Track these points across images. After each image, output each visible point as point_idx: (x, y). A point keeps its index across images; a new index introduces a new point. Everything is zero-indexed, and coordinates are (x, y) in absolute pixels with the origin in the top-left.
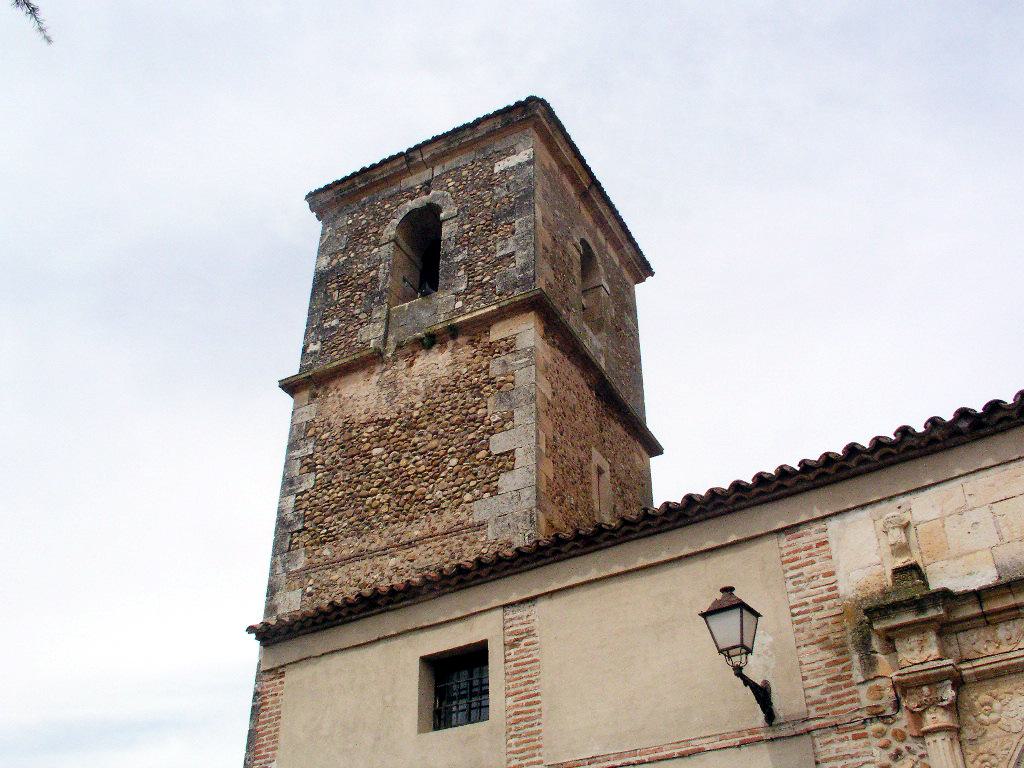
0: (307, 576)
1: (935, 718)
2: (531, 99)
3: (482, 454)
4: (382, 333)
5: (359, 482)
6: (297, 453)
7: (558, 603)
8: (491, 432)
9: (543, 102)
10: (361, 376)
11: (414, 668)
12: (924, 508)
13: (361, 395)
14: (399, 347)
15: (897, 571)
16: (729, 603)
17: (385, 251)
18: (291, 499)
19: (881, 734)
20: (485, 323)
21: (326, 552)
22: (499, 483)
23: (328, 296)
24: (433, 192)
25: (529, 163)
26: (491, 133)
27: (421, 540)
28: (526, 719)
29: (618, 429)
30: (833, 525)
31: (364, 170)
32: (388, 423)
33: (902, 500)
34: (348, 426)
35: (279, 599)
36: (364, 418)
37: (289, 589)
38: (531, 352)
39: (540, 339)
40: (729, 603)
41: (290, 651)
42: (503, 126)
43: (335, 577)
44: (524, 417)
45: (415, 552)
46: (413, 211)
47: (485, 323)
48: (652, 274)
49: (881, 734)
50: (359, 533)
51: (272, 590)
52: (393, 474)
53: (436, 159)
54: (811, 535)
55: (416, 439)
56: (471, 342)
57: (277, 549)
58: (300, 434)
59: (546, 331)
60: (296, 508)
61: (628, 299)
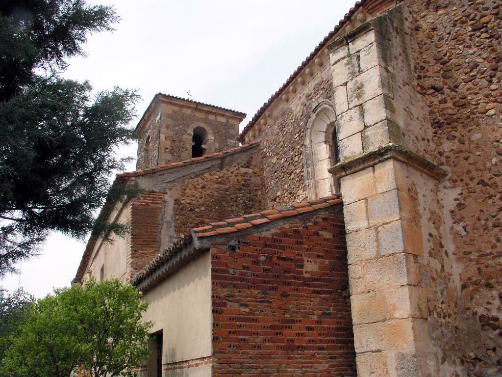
2: (157, 95)
9: (160, 94)
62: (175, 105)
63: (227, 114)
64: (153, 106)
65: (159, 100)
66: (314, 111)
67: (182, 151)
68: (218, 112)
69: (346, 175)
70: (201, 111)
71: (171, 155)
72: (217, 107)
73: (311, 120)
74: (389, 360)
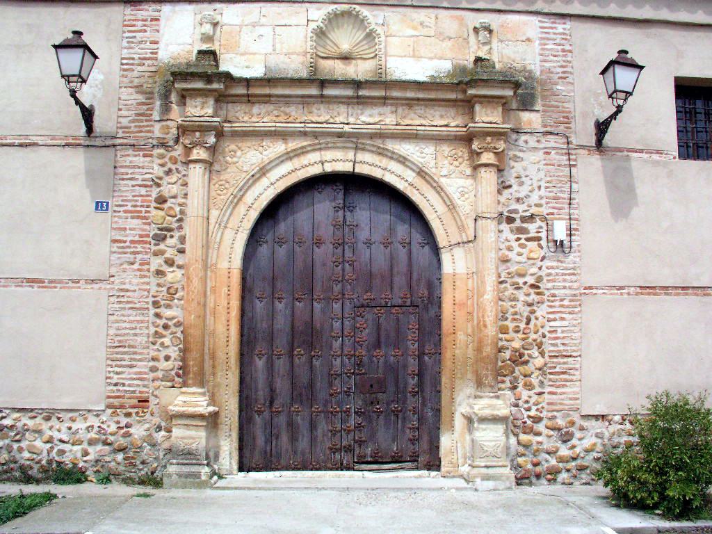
19: (161, 156)
40: (76, 43)
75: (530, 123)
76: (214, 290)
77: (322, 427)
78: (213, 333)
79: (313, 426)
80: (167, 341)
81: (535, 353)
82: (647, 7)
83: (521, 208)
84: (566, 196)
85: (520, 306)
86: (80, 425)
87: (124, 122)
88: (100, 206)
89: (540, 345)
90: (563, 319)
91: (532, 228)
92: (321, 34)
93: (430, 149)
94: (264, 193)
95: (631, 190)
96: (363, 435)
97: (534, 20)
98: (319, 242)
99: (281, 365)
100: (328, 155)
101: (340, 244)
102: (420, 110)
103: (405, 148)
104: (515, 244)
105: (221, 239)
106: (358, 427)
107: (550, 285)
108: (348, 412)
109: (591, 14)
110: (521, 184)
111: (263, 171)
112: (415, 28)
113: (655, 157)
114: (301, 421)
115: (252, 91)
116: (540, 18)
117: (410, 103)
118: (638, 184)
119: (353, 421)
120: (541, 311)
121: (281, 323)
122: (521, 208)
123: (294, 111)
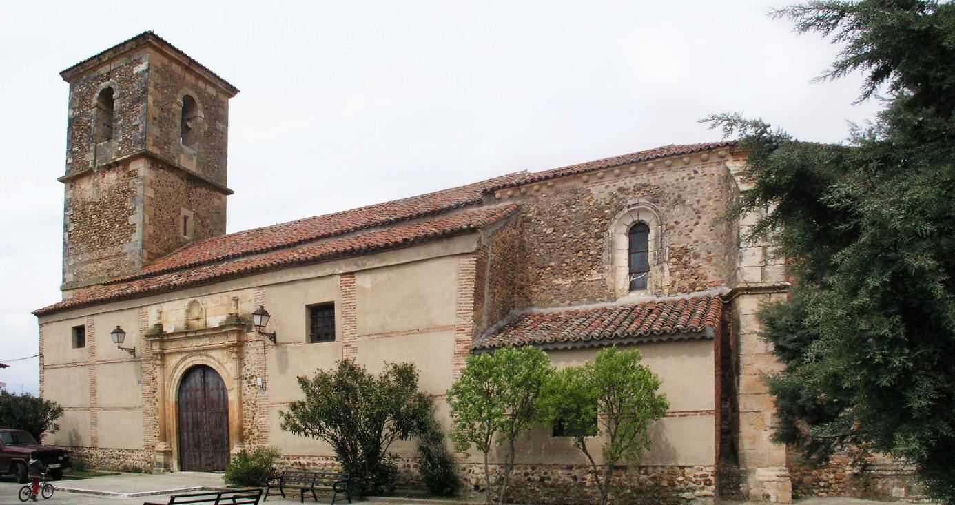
0: (74, 267)
1: (158, 362)
2: (146, 33)
3: (126, 224)
4: (93, 158)
5: (88, 230)
6: (67, 213)
7: (99, 316)
8: (129, 214)
9: (151, 34)
10: (86, 179)
11: (70, 330)
12: (165, 307)
13: (87, 186)
14: (98, 169)
15: (156, 325)
16: (119, 331)
17: (93, 111)
18: (67, 234)
19: (152, 363)
20: (126, 163)
21: (80, 258)
22: (131, 237)
23: (74, 133)
24: (111, 80)
25: (147, 71)
26: (132, 49)
27: (108, 257)
28: (92, 348)
29: (203, 191)
30: (149, 307)
31: (81, 63)
32: (97, 204)
33: (161, 304)
34: (84, 203)
35: (66, 276)
36: (88, 200)
37: (69, 272)
38: (143, 179)
39: (147, 170)
40: (119, 331)
41: (44, 320)
42: (136, 46)
43: (83, 269)
44: (139, 210)
45: (107, 262)
46: (103, 90)
47: (126, 163)
48: (232, 91)
49: (152, 363)
50: (89, 252)
51: (64, 273)
52: (99, 227)
53: (110, 61)
54: (144, 310)
55: (106, 213)
56: (124, 169)
57: (64, 256)
58: (68, 205)
59: (152, 164)
60: (69, 238)
61: (221, 112)
62: (165, 55)
63: (219, 85)
64: (128, 45)
65: (148, 42)
66: (629, 207)
67: (171, 127)
68: (211, 80)
69: (747, 294)
70: (192, 72)
71: (159, 129)
72: (212, 73)
73: (622, 213)
74: (765, 418)
75: (251, 337)
76: (169, 409)
77: (203, 457)
78: (169, 424)
79: (200, 456)
80: (158, 427)
81: (256, 430)
82: (312, 272)
83: (249, 373)
84: (263, 366)
85: (250, 413)
86: (140, 455)
87: (143, 352)
88: (139, 382)
89: (257, 427)
90: (264, 417)
91: (253, 381)
92: (188, 311)
93: (220, 352)
94: (179, 374)
95: (287, 361)
96: (213, 460)
97: (252, 290)
98: (197, 391)
99: (191, 434)
100: (193, 358)
101: (218, 389)
102: (217, 338)
103: (213, 353)
104: (248, 388)
105: (586, 345)
106: (212, 457)
107: (259, 403)
108: (209, 451)
109: (320, 275)
110: (249, 363)
111: (177, 366)
112: (214, 303)
113: (297, 345)
114: (197, 454)
115: (188, 335)
116: (255, 289)
117: (214, 335)
118: (289, 358)
119: (211, 454)
120: (257, 414)
121: (190, 420)
122: (249, 373)
123: (183, 343)
